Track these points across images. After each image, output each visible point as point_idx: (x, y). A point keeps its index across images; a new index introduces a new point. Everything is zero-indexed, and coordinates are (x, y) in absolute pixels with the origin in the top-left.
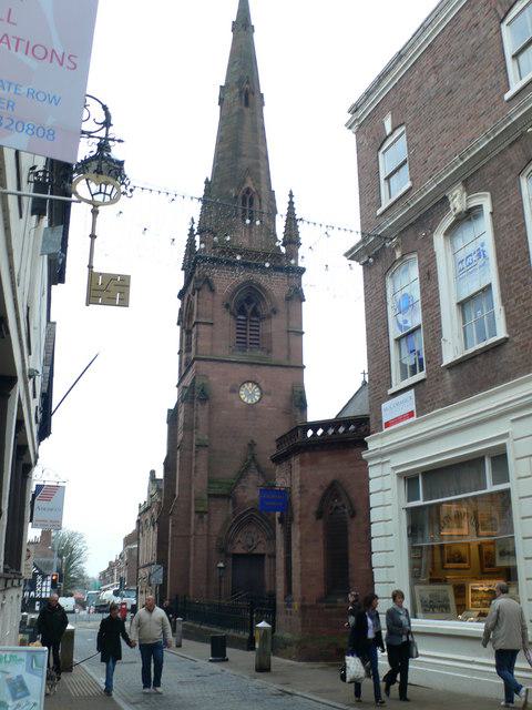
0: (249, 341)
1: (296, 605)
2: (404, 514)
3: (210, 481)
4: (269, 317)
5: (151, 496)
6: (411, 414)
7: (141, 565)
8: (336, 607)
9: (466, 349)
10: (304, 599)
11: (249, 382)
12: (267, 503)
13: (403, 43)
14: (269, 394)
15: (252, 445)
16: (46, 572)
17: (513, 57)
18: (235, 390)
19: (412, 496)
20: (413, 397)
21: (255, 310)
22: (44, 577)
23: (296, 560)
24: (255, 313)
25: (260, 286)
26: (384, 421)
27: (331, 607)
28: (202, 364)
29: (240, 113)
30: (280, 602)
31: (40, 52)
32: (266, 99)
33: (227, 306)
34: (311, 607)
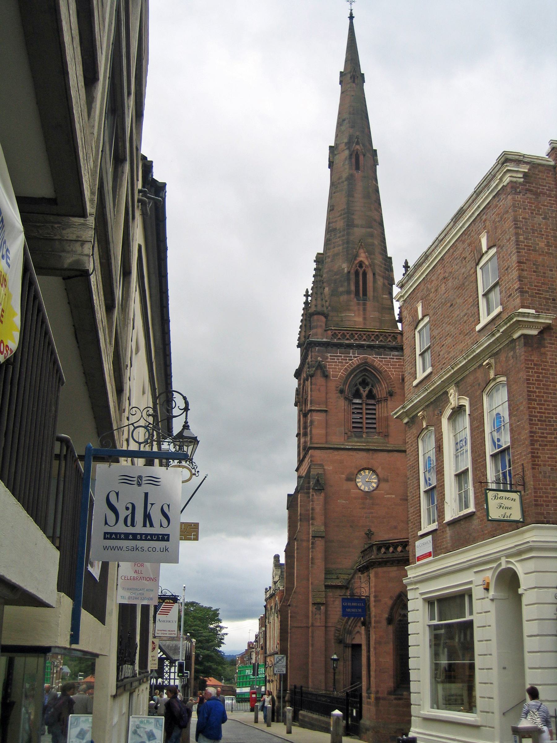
0: (365, 426)
1: (373, 696)
2: (427, 628)
3: (328, 572)
4: (386, 400)
5: (275, 583)
6: (429, 555)
7: (268, 652)
9: (461, 510)
10: (377, 692)
11: (366, 469)
12: (349, 610)
13: (439, 232)
14: (386, 481)
16: (175, 657)
17: (483, 295)
18: (351, 479)
19: (432, 618)
21: (370, 391)
22: (172, 662)
23: (372, 659)
24: (371, 395)
26: (417, 556)
27: (400, 699)
28: (317, 453)
29: (351, 178)
30: (364, 694)
31: (148, 579)
32: (380, 157)
33: (342, 392)
34: (384, 699)
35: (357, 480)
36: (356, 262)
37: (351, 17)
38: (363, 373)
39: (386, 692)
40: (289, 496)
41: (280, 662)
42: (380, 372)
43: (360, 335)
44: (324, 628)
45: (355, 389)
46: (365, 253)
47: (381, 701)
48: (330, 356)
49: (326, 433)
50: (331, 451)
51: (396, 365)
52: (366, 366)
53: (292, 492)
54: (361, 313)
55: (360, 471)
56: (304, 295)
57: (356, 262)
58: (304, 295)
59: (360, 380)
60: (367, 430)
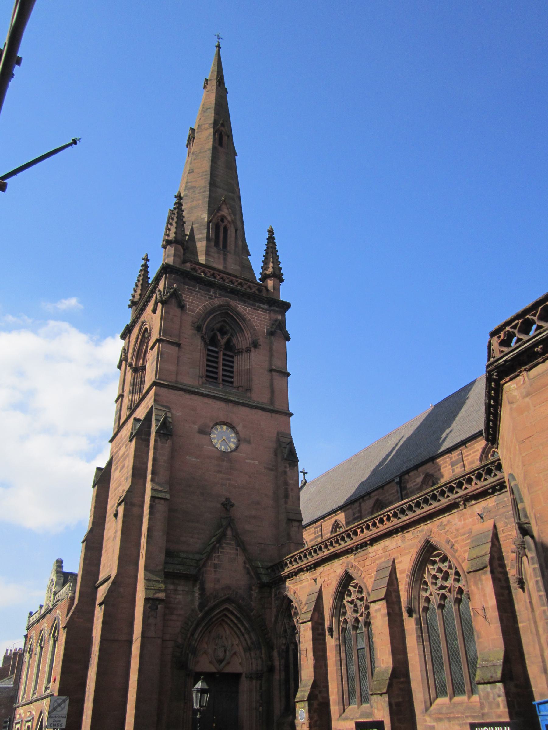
4: (248, 350)
14: (248, 442)
15: (227, 505)
18: (205, 431)
24: (229, 346)
25: (238, 314)
33: (199, 329)
35: (212, 436)
36: (219, 214)
37: (219, 47)
38: (223, 319)
40: (99, 469)
41: (59, 709)
42: (244, 319)
44: (159, 641)
45: (212, 333)
46: (228, 209)
48: (188, 288)
50: (182, 393)
51: (261, 318)
52: (227, 309)
54: (222, 261)
55: (217, 424)
56: (176, 197)
57: (219, 214)
59: (218, 325)
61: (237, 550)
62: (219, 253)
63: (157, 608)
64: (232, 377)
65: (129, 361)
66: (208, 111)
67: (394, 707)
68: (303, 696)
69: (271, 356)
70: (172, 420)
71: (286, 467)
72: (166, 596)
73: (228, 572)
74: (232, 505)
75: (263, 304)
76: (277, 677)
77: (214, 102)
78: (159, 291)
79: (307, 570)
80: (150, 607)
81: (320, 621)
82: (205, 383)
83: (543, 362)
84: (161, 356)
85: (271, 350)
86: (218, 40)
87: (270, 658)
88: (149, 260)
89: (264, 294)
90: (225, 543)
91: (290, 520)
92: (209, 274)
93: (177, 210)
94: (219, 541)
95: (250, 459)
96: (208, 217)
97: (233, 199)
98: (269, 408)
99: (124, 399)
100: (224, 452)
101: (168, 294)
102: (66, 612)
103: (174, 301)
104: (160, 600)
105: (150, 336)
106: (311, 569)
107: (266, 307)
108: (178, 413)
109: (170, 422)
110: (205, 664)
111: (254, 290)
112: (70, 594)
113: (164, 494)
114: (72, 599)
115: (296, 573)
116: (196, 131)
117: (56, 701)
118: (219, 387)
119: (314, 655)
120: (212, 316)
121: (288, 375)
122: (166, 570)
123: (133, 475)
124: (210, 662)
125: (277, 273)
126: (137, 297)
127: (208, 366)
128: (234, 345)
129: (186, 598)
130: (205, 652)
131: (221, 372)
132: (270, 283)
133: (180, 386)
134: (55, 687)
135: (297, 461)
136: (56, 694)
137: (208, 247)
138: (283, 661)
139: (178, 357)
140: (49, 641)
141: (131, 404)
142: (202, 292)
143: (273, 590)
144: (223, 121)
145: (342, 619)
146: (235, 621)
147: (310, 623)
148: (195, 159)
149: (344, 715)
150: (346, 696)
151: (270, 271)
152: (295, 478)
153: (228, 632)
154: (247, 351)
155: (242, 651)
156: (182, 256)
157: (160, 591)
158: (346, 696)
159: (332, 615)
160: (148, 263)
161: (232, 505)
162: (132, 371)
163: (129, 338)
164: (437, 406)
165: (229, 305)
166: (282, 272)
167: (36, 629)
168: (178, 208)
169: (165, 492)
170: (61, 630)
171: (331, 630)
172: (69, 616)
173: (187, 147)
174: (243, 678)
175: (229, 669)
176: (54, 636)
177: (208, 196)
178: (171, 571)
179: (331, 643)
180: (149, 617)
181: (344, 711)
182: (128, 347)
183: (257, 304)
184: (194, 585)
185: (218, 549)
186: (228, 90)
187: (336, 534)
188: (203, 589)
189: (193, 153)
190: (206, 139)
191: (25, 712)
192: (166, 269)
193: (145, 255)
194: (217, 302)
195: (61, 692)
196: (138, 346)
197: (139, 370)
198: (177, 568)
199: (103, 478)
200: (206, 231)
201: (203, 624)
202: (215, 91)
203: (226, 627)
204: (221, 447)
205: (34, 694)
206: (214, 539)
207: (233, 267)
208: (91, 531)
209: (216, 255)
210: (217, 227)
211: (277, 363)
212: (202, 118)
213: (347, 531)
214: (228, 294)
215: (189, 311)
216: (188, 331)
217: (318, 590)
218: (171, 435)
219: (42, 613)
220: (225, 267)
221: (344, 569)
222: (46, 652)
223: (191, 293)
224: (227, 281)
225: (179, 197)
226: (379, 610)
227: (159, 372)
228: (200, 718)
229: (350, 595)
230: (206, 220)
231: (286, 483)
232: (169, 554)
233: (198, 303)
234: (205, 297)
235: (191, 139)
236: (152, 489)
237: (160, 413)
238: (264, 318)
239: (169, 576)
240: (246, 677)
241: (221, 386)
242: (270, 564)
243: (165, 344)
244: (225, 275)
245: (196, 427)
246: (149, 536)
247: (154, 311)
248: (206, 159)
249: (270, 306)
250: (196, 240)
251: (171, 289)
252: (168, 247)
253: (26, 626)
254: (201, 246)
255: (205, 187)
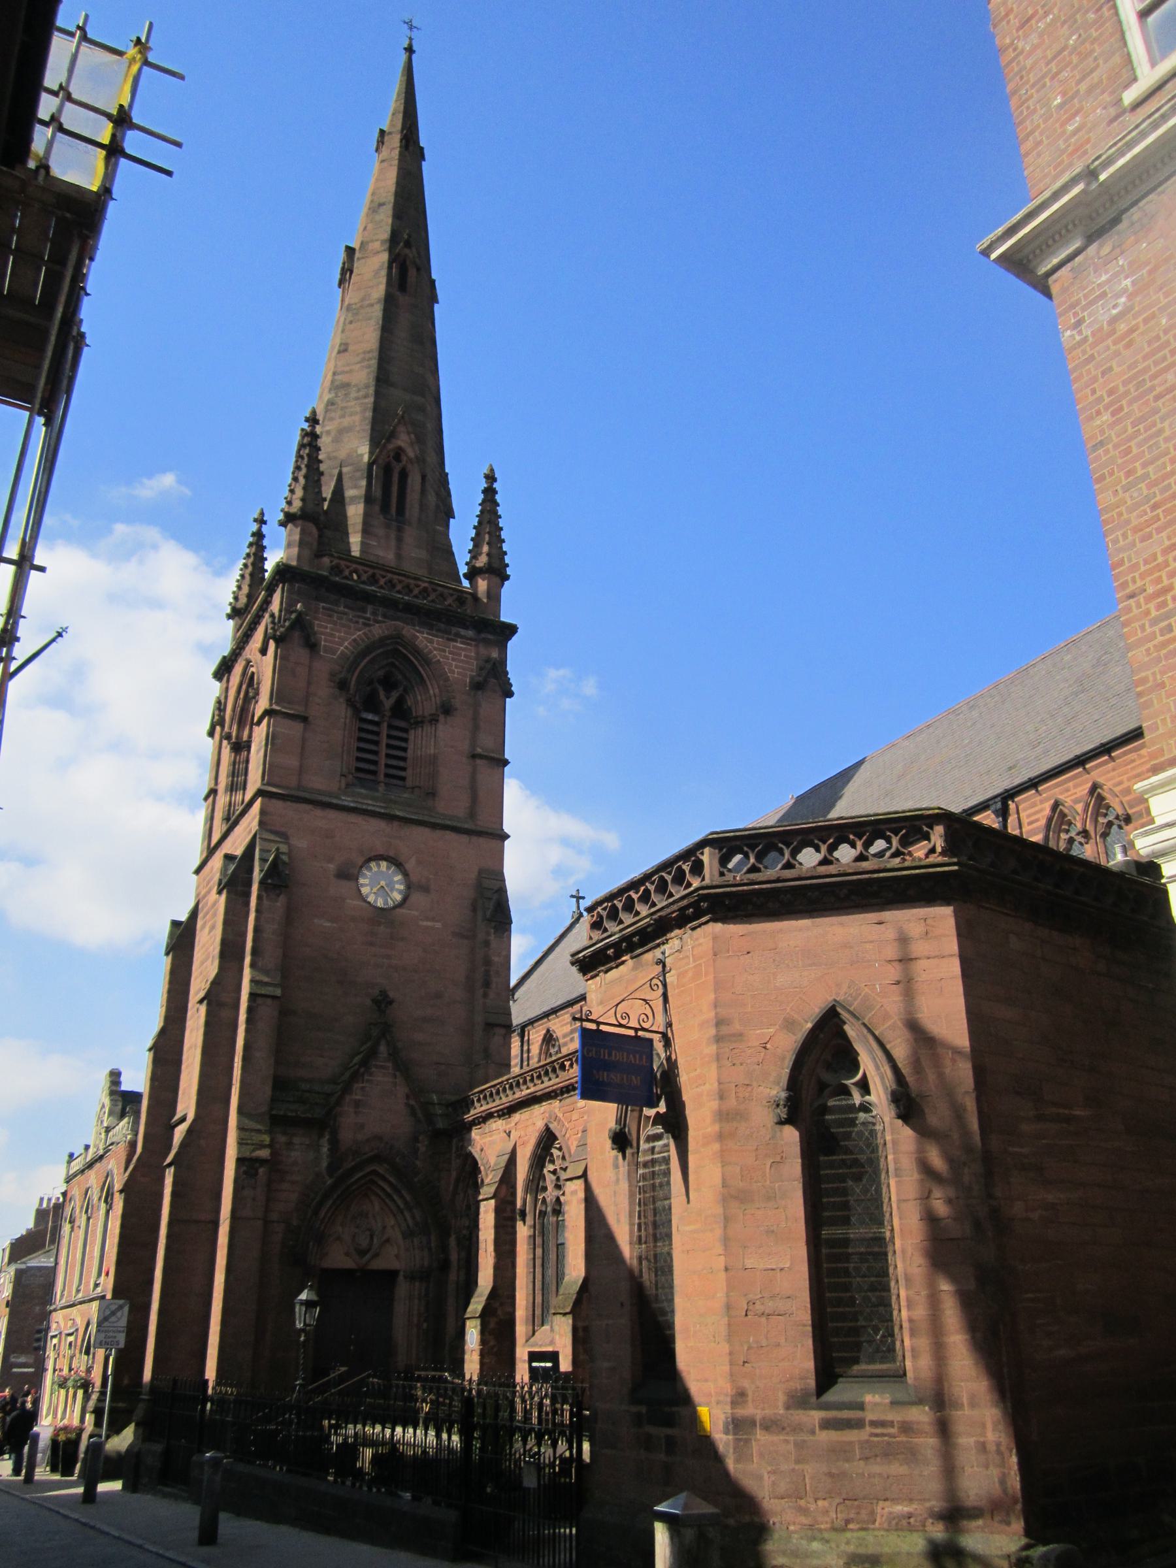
0: (382, 770)
4: (434, 720)
8: (859, 1424)
10: (740, 1397)
14: (425, 889)
15: (383, 1002)
18: (349, 875)
20: (513, 1017)
21: (400, 701)
24: (400, 710)
25: (417, 652)
27: (848, 1425)
33: (343, 685)
34: (770, 1425)
35: (361, 881)
36: (391, 446)
37: (410, 50)
38: (390, 660)
39: (781, 1398)
40: (175, 924)
41: (113, 1319)
42: (426, 661)
43: (390, 581)
44: (260, 1223)
45: (368, 688)
46: (409, 433)
47: (760, 1435)
48: (324, 608)
49: (301, 766)
50: (307, 807)
52: (398, 643)
53: (183, 917)
54: (393, 543)
55: (370, 860)
56: (255, 520)
57: (391, 446)
58: (255, 520)
59: (381, 673)
60: (387, 780)
61: (395, 1076)
62: (388, 526)
63: (256, 1174)
64: (404, 769)
65: (226, 729)
66: (382, 209)
67: (581, 1334)
68: (475, 1311)
69: (476, 728)
70: (290, 858)
71: (488, 934)
72: (272, 1154)
73: (379, 1111)
74: (391, 1002)
75: (467, 628)
76: (453, 1277)
77: (392, 189)
78: (272, 615)
79: (499, 1117)
80: (245, 1173)
81: (510, 1198)
82: (353, 785)
83: (617, 967)
84: (272, 740)
85: (475, 718)
86: (408, 33)
87: (444, 1248)
88: (265, 523)
89: (469, 609)
90: (376, 1066)
91: (489, 1026)
92: (364, 577)
93: (307, 451)
94: (365, 1063)
95: (427, 919)
96: (371, 453)
97: (422, 409)
98: (466, 826)
99: (218, 798)
100: (382, 909)
101: (287, 624)
102: (123, 1165)
103: (297, 634)
104: (262, 1162)
105: (257, 694)
106: (504, 1115)
107: (470, 633)
108: (301, 843)
109: (284, 863)
110: (338, 1258)
111: (449, 601)
112: (129, 1137)
113: (271, 989)
114: (133, 1145)
115: (488, 1116)
116: (357, 255)
117: (107, 1307)
118: (377, 791)
119: (496, 1250)
120: (368, 659)
121: (506, 763)
122: (274, 1112)
123: (223, 955)
124: (347, 1254)
125: (496, 565)
126: (243, 600)
127: (359, 749)
128: (410, 709)
129: (306, 1157)
130: (339, 1238)
131: (383, 761)
132: (482, 585)
133: (306, 795)
134: (107, 1284)
135: (511, 922)
136: (109, 1296)
137: (367, 515)
138: (463, 1254)
139: (304, 740)
140: (98, 1209)
141: (229, 810)
142: (351, 614)
143: (455, 1141)
144: (410, 236)
145: (540, 1197)
146: (389, 1190)
147: (493, 1201)
148: (351, 322)
149: (532, 1340)
150: (538, 1312)
151: (482, 561)
152: (504, 953)
153: (377, 1207)
154: (430, 721)
155: (400, 1236)
156: (315, 544)
157: (261, 1146)
158: (538, 1312)
159: (527, 1190)
160: (265, 529)
161: (391, 1002)
162: (232, 749)
163: (228, 681)
164: (800, 800)
165: (397, 638)
166: (507, 560)
167: (79, 1184)
168: (309, 444)
169: (275, 985)
170: (117, 1195)
171: (523, 1214)
172: (127, 1174)
173: (340, 286)
174: (401, 1278)
175: (379, 1264)
176: (106, 1201)
177: (370, 406)
178: (282, 1113)
179: (523, 1231)
180: (243, 1188)
181: (534, 1334)
182: (226, 697)
183: (454, 630)
184: (321, 1136)
185: (363, 1075)
186: (426, 151)
187: (548, 1060)
188: (334, 1143)
189: (349, 308)
190: (374, 271)
191: (65, 1318)
192: (283, 571)
193: (258, 511)
194: (378, 631)
195: (118, 1292)
196: (240, 702)
197: (240, 747)
198: (292, 1104)
199: (182, 938)
200: (364, 483)
201: (335, 1196)
202: (396, 162)
203: (373, 1198)
204: (376, 901)
205: (78, 1291)
206: (357, 1059)
207: (414, 556)
208: (163, 1032)
209: (381, 532)
210: (387, 470)
211: (486, 742)
212: (370, 226)
213: (553, 1062)
214: (399, 614)
215: (325, 651)
216: (323, 690)
217: (509, 1149)
218: (286, 887)
219: (88, 1159)
220: (399, 556)
221: (545, 1121)
222: (95, 1225)
223: (330, 616)
224: (399, 587)
225: (313, 420)
226: (574, 1192)
227: (270, 771)
228: (305, 1341)
229: (552, 1162)
230: (366, 458)
231: (488, 962)
232: (280, 1085)
233: (341, 635)
234: (357, 622)
235: (347, 271)
236: (252, 981)
237: (267, 846)
238: (466, 656)
239: (278, 1122)
240: (405, 1277)
241: (381, 788)
242: (453, 1098)
243: (279, 718)
244: (396, 577)
245: (331, 866)
246: (245, 1059)
247: (264, 651)
248: (372, 322)
249: (479, 632)
250: (347, 500)
251: (292, 612)
252: (290, 526)
253: (63, 1175)
254: (355, 512)
255: (367, 387)
